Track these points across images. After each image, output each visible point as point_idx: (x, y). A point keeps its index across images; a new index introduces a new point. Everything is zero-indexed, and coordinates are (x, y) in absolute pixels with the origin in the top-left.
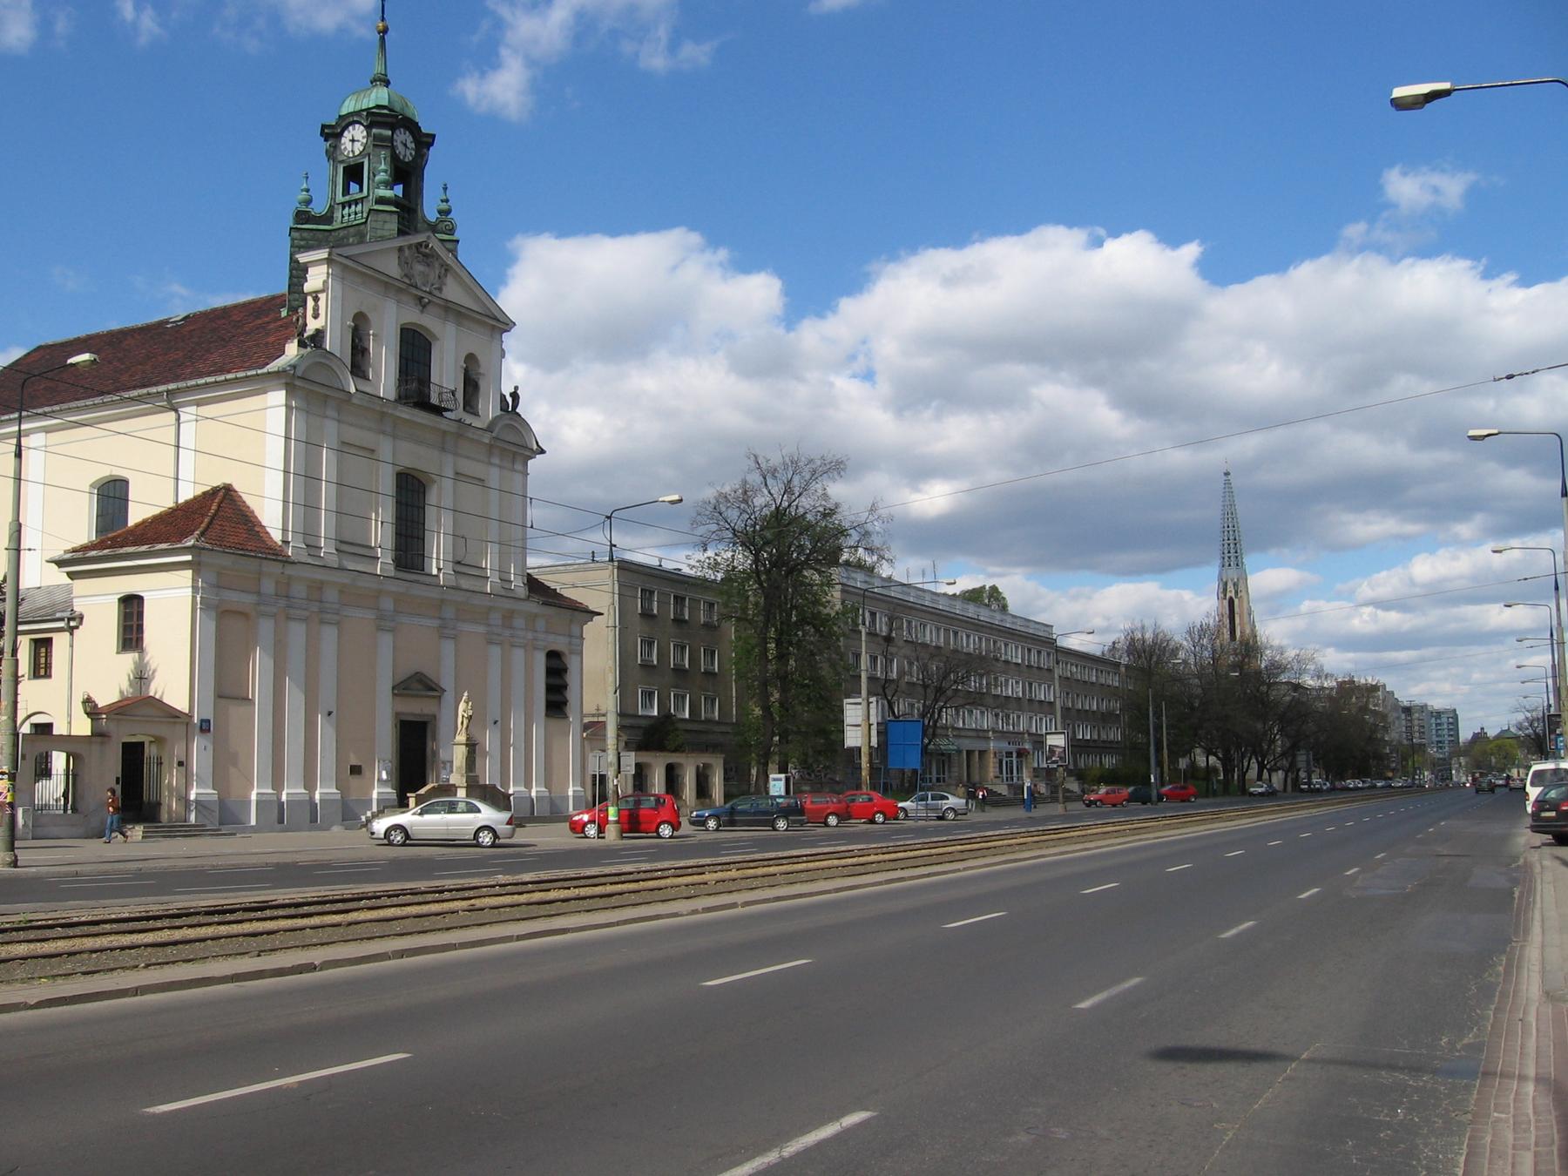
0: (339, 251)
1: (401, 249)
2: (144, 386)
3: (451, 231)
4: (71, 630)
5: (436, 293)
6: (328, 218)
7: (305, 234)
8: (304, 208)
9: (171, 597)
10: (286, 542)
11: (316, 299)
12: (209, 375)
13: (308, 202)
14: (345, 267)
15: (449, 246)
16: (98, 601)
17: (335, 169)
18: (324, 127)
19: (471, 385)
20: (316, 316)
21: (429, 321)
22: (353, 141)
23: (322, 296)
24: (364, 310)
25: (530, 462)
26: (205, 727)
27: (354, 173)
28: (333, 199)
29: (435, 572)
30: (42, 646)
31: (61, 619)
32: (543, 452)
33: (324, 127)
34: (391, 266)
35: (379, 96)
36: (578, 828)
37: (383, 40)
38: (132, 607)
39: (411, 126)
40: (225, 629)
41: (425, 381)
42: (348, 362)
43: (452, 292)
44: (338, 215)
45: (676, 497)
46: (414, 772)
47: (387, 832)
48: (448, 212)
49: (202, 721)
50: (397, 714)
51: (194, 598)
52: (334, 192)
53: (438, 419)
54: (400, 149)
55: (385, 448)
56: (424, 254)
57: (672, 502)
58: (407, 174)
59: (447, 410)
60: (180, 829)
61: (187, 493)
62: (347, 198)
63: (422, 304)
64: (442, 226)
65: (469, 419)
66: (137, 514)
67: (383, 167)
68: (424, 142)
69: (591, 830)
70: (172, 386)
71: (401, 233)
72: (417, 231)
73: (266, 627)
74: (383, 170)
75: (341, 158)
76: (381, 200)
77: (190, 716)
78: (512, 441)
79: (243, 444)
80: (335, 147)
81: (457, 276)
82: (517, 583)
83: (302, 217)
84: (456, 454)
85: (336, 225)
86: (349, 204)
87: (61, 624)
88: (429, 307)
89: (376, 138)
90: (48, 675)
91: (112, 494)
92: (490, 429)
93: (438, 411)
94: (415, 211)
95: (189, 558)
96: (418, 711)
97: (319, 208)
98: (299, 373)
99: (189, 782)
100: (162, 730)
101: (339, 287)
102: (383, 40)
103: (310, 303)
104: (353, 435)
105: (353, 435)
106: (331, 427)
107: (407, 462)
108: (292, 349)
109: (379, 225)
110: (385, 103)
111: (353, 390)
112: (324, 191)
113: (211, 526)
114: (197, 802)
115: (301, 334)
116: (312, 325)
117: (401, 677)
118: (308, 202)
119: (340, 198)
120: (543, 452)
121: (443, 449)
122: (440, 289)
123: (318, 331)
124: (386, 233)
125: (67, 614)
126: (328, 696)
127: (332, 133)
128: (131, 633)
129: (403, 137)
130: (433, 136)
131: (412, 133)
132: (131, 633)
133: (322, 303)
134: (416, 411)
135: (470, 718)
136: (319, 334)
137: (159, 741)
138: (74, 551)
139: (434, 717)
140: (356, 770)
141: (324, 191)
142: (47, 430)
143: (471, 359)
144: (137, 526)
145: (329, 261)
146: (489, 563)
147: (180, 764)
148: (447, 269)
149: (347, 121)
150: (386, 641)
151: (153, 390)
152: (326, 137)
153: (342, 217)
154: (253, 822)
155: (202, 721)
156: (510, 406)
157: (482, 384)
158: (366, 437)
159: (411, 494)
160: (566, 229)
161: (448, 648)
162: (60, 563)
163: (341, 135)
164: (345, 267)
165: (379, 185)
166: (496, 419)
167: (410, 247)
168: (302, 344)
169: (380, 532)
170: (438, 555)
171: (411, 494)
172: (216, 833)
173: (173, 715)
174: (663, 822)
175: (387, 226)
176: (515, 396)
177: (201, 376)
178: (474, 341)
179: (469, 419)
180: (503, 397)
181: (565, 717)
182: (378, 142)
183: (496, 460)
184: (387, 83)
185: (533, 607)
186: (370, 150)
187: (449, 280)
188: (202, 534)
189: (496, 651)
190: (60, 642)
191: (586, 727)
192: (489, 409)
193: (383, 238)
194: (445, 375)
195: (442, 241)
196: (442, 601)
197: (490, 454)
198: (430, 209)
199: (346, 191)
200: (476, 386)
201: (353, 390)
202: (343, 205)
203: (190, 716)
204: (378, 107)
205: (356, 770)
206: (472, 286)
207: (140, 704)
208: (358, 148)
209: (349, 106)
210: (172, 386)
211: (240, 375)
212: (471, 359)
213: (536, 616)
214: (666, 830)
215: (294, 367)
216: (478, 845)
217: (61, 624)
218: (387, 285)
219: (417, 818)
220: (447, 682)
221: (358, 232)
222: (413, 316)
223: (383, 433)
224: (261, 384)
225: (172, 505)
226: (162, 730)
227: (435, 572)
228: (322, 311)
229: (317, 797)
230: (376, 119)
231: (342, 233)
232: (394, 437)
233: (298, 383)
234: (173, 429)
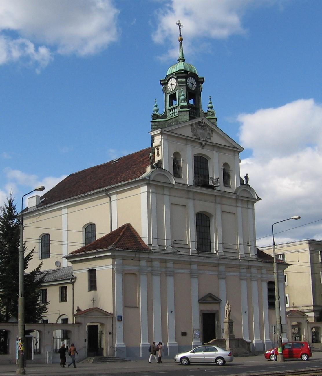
0: (165, 129)
1: (191, 125)
2: (99, 188)
3: (214, 115)
4: (73, 283)
5: (209, 140)
6: (165, 116)
7: (156, 123)
8: (156, 113)
9: (105, 268)
10: (150, 245)
11: (158, 149)
12: (120, 182)
13: (157, 111)
14: (168, 135)
15: (212, 121)
16: (81, 272)
17: (166, 96)
18: (161, 81)
19: (227, 176)
20: (158, 156)
21: (206, 152)
22: (172, 85)
23: (160, 148)
24: (178, 151)
25: (255, 204)
26: (119, 319)
27: (173, 97)
28: (166, 108)
29: (215, 252)
30: (63, 290)
31: (69, 279)
32: (260, 199)
33: (161, 81)
34: (188, 132)
35: (180, 66)
36: (268, 356)
37: (181, 44)
38: (92, 273)
39: (194, 76)
40: (126, 279)
41: (207, 176)
42: (172, 172)
43: (215, 139)
44: (168, 114)
45: (297, 217)
46: (209, 332)
47: (182, 359)
48: (212, 107)
49: (118, 317)
50: (201, 311)
51: (113, 269)
52: (166, 105)
53: (212, 191)
54: (190, 86)
55: (191, 204)
56: (202, 125)
57: (296, 219)
58: (194, 94)
59: (215, 187)
60: (112, 359)
61: (115, 228)
62: (171, 107)
63: (202, 145)
64: (209, 113)
65: (227, 190)
66: (98, 237)
67: (182, 94)
68: (200, 81)
69: (273, 358)
70: (107, 188)
71: (191, 118)
72: (199, 116)
73: (143, 279)
74: (182, 94)
75: (168, 92)
76: (182, 107)
77: (113, 315)
78: (247, 196)
79: (132, 208)
80: (166, 88)
81: (218, 133)
82: (252, 254)
83: (155, 117)
84: (221, 204)
85: (168, 118)
86: (172, 109)
87: (69, 281)
88: (206, 147)
89: (179, 82)
90: (66, 301)
91: (90, 229)
92: (235, 193)
93: (212, 187)
94: (199, 109)
95: (110, 254)
96: (210, 309)
97: (161, 112)
98: (152, 178)
99: (114, 340)
100: (103, 321)
101: (166, 143)
102: (181, 44)
103: (156, 151)
104: (176, 200)
105: (176, 200)
106: (167, 198)
107: (199, 210)
108: (149, 170)
109: (182, 117)
110: (183, 68)
111: (174, 183)
112: (162, 105)
113: (123, 240)
114: (117, 349)
115: (152, 163)
116: (157, 159)
117: (203, 294)
118: (157, 111)
119: (169, 108)
120: (260, 199)
121: (216, 203)
122: (210, 139)
123: (159, 161)
124: (185, 120)
125: (71, 277)
126: (170, 305)
127: (164, 83)
128: (93, 285)
129: (191, 80)
130: (203, 78)
131: (194, 78)
132: (93, 285)
133: (160, 150)
134: (202, 188)
135: (230, 311)
136: (160, 162)
137: (102, 324)
138: (72, 253)
139: (218, 311)
140: (184, 334)
141: (162, 105)
142: (68, 207)
143: (226, 165)
144: (98, 240)
145: (161, 134)
146: (239, 248)
147: (110, 333)
148: (212, 130)
149: (169, 77)
150: (195, 282)
151: (101, 190)
152: (162, 84)
153: (171, 115)
154: (141, 356)
155: (118, 317)
156: (245, 183)
157: (231, 174)
158: (183, 201)
159: (203, 221)
160: (252, 110)
161: (223, 283)
162: (67, 258)
163: (167, 83)
164: (168, 135)
165: (181, 102)
166: (238, 188)
167: (195, 123)
168: (152, 167)
169: (190, 237)
170: (216, 247)
171: (203, 221)
172: (123, 360)
173: (106, 315)
174: (303, 354)
175: (185, 117)
176: (247, 178)
177: (117, 182)
178: (226, 157)
179: (227, 190)
180: (241, 179)
181: (275, 309)
182: (180, 84)
183: (239, 205)
184: (184, 60)
185: (260, 264)
186: (177, 88)
187: (214, 135)
188: (115, 244)
189: (244, 284)
190: (69, 288)
191: (288, 313)
192: (235, 184)
193: (184, 122)
194: (215, 173)
195: (208, 119)
196: (219, 264)
197: (237, 203)
198: (204, 107)
199: (171, 104)
200: (229, 176)
201: (174, 183)
202: (170, 110)
203: (113, 315)
204: (180, 70)
205: (184, 334)
206: (223, 135)
207: (95, 311)
208: (174, 87)
209: (170, 71)
210: (107, 188)
211: (117, 185)
212: (226, 165)
213: (261, 267)
214: (305, 357)
215: (149, 176)
216: (217, 365)
217: (69, 281)
218: (186, 139)
219: (192, 354)
220: (222, 296)
221: (176, 120)
222: (198, 150)
223: (189, 198)
224: (137, 184)
225: (108, 232)
226: (103, 321)
227: (215, 252)
228: (160, 153)
229: (168, 345)
230: (178, 75)
231: (170, 121)
232: (194, 199)
233: (151, 182)
234: (109, 204)
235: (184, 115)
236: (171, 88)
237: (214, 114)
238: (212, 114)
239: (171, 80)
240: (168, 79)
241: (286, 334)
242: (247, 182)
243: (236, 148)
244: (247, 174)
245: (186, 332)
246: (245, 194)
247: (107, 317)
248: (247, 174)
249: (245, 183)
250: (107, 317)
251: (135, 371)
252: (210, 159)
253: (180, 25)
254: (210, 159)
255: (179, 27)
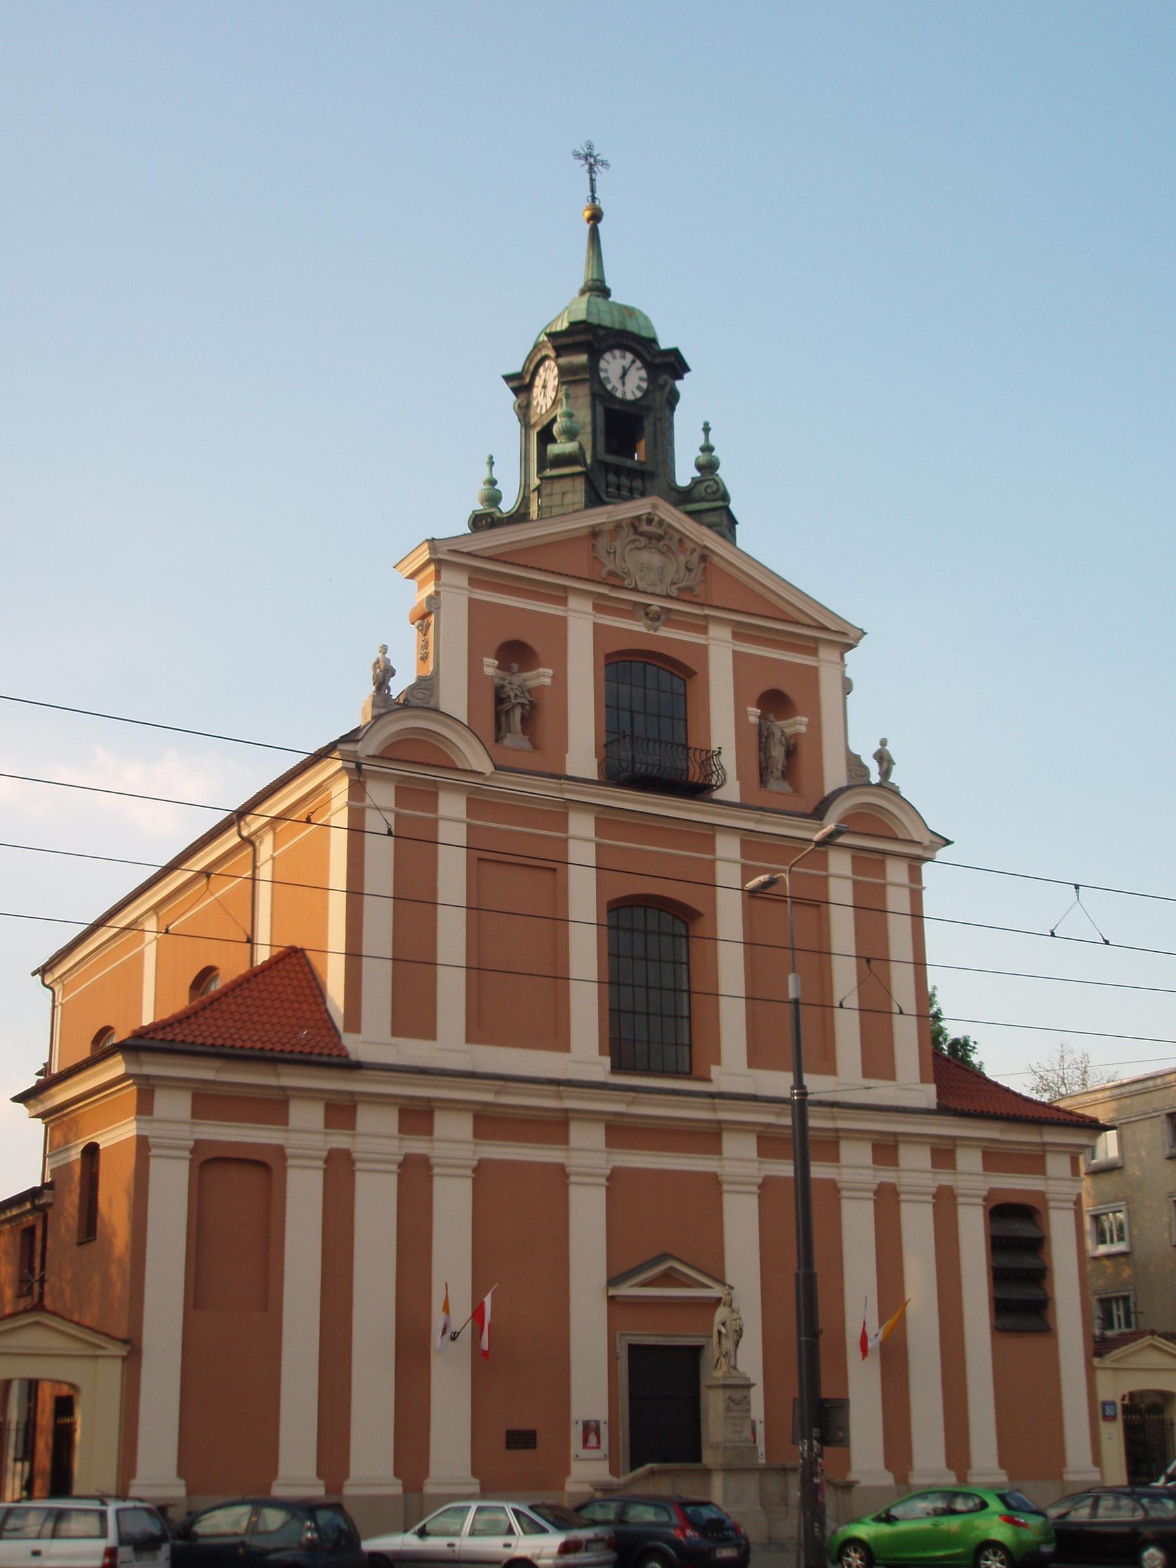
39: (641, 346)
64: (701, 489)
68: (668, 366)
175: (569, 499)
176: (884, 759)
235: (564, 493)
236: (542, 402)
237: (718, 490)
238: (709, 490)
239: (541, 370)
240: (532, 368)
241: (1069, 1477)
242: (885, 774)
243: (825, 629)
244: (883, 743)
245: (508, 1447)
246: (731, 1404)
247: (96, 1357)
248: (883, 743)
249: (875, 778)
250: (96, 1357)
251: (269, 1546)
252: (845, 638)
253: (592, 160)
254: (845, 638)
255: (587, 167)
